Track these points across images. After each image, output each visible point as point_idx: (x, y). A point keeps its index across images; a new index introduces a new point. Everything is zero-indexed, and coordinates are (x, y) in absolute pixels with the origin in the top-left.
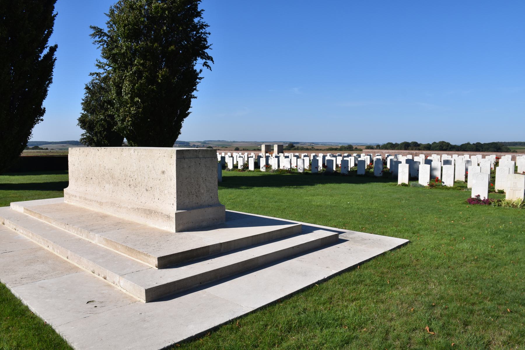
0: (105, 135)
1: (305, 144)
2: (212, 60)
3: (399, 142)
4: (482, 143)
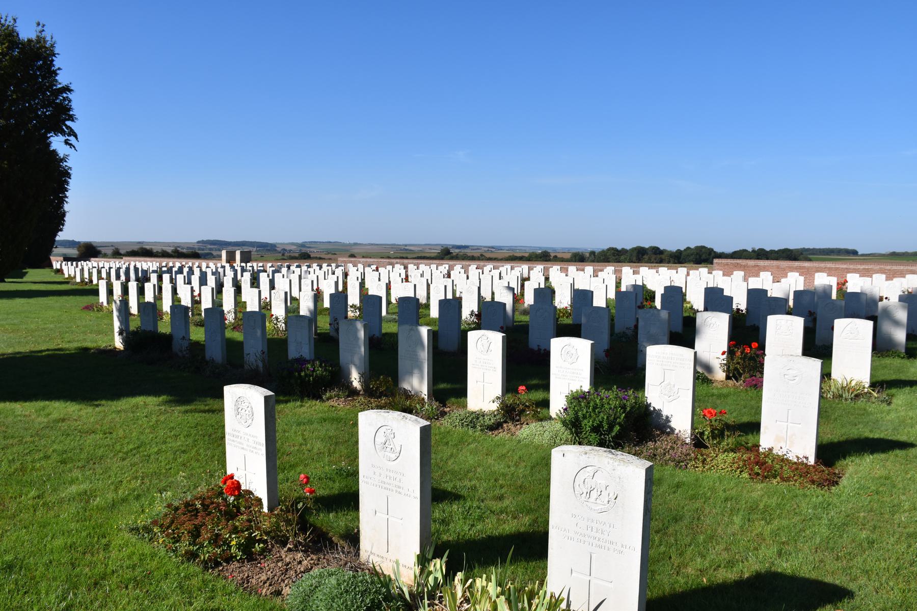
2: (76, 136)
4: (768, 249)
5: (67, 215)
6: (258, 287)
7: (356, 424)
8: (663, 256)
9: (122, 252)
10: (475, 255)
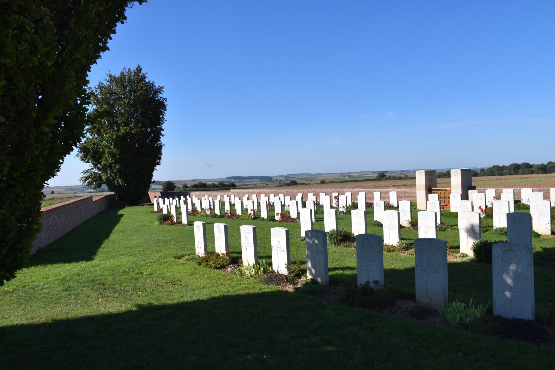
0: (118, 170)
1: (395, 172)
3: (507, 163)
5: (164, 148)
6: (549, 199)
8: (533, 169)
9: (189, 186)
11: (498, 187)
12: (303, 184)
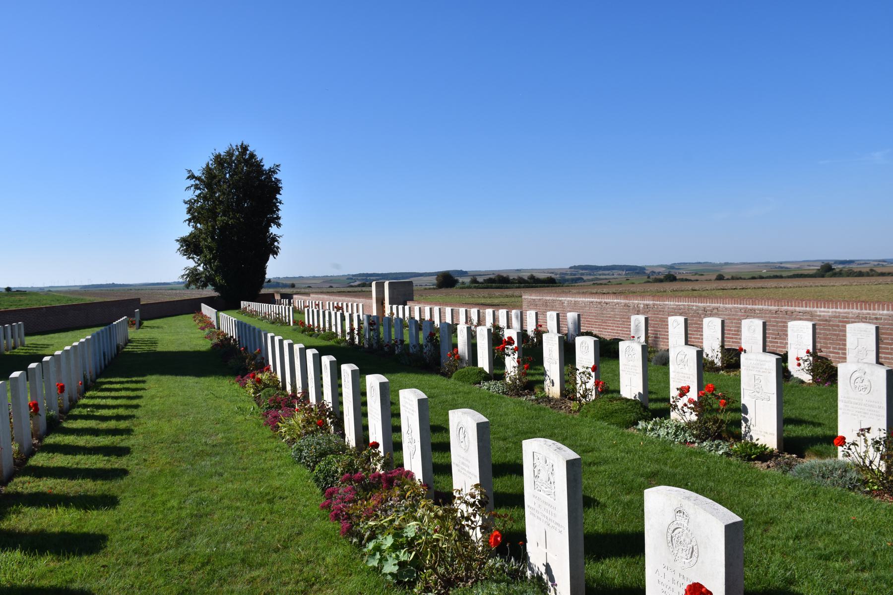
1: (866, 262)
7: (521, 447)
9: (480, 279)
10: (864, 270)
11: (455, 306)
12: (687, 280)
